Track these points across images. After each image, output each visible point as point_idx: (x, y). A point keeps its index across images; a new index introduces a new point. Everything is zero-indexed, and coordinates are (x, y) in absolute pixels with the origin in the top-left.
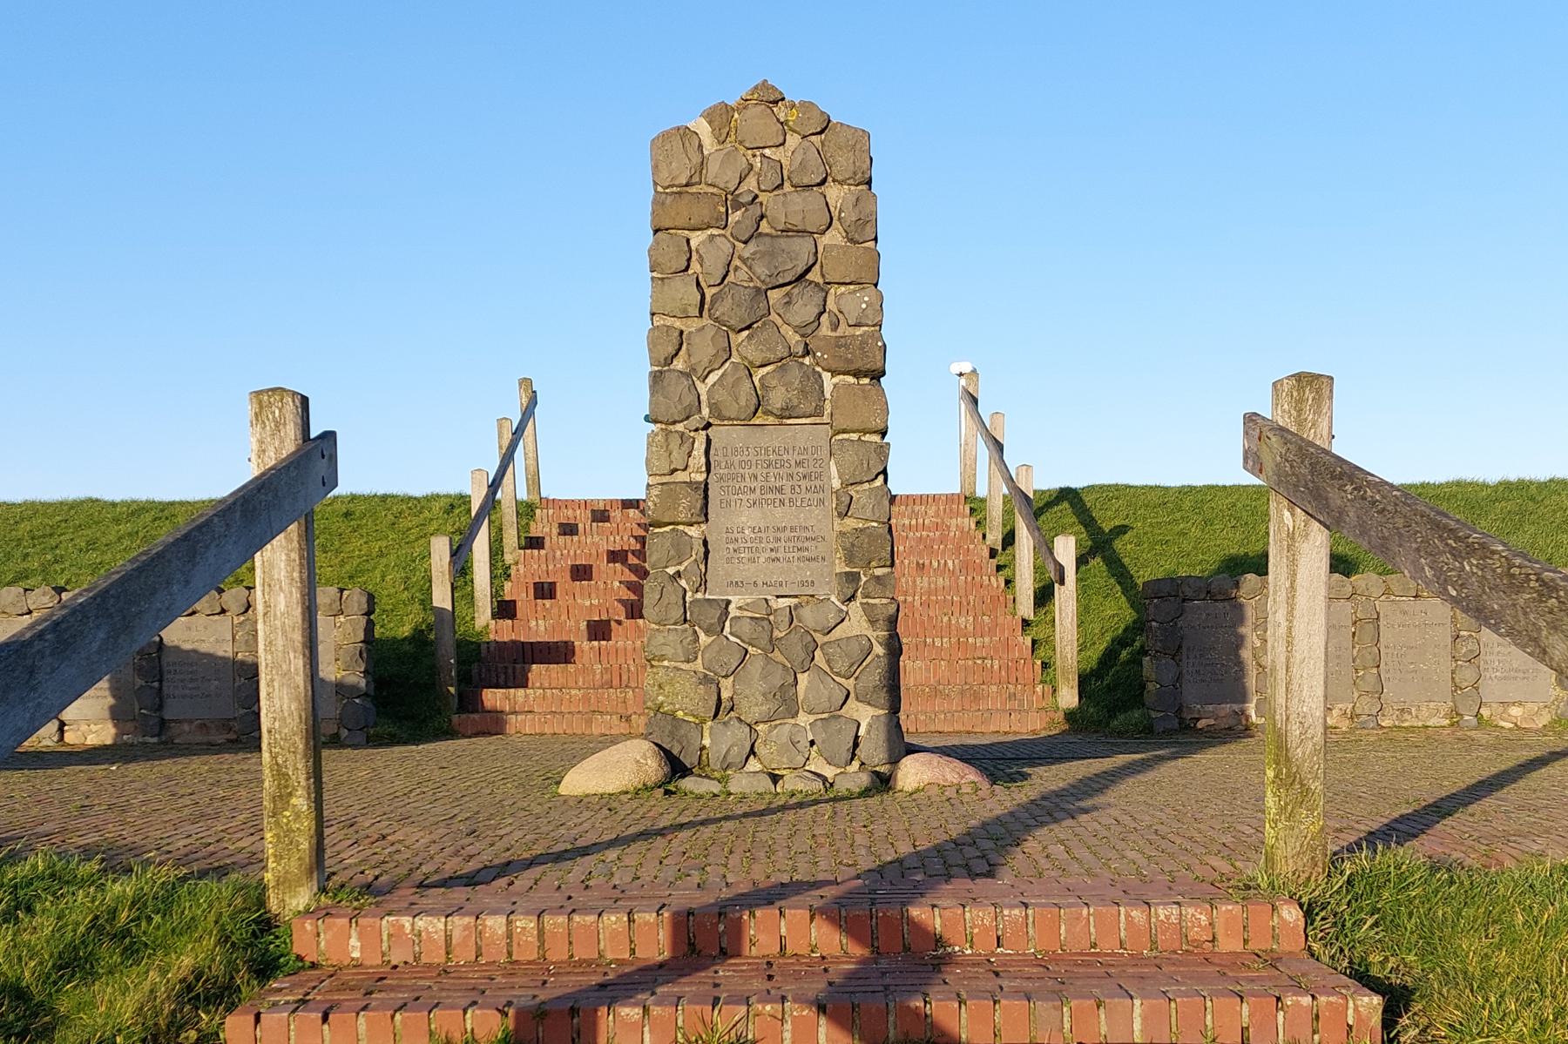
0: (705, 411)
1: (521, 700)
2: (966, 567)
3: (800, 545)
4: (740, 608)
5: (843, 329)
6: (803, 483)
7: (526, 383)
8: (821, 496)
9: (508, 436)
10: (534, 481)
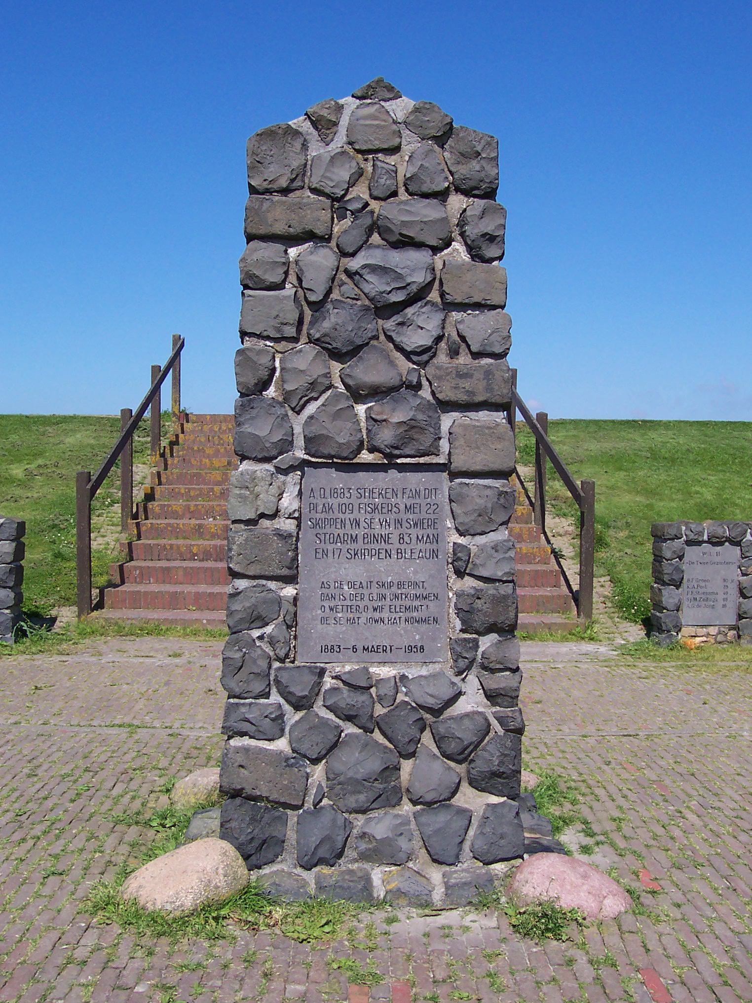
3: (408, 603)
6: (414, 532)
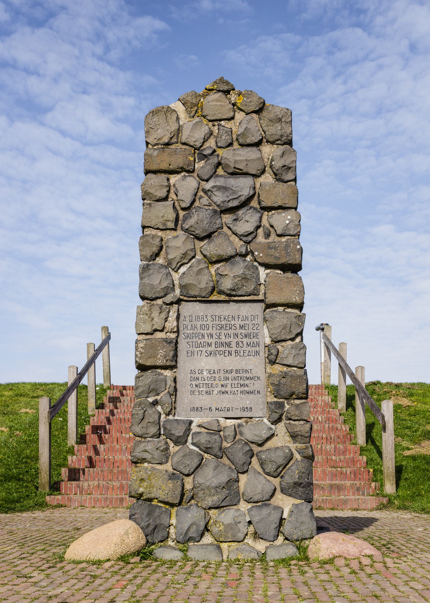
0: (178, 291)
1: (86, 488)
2: (329, 419)
3: (242, 382)
4: (199, 426)
5: (273, 237)
6: (245, 340)
7: (105, 329)
8: (257, 349)
9: (92, 352)
10: (108, 376)
